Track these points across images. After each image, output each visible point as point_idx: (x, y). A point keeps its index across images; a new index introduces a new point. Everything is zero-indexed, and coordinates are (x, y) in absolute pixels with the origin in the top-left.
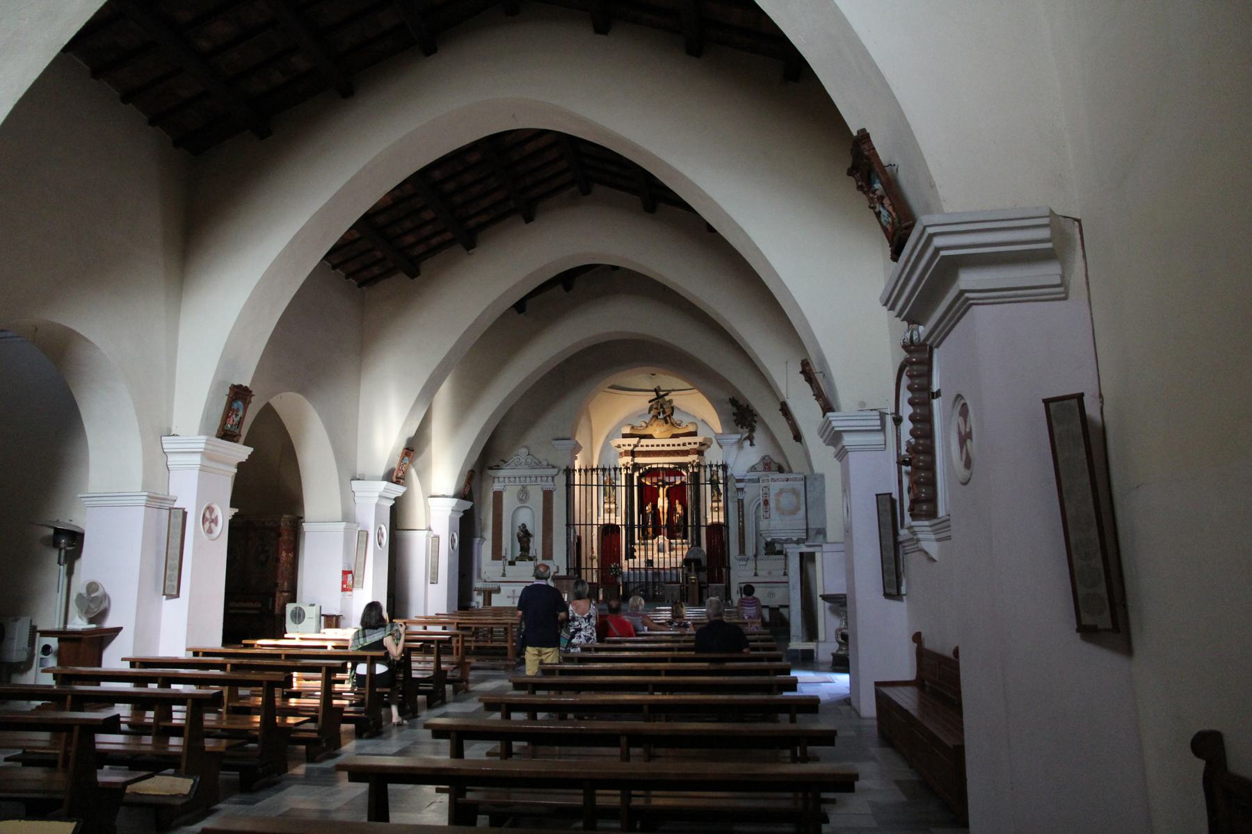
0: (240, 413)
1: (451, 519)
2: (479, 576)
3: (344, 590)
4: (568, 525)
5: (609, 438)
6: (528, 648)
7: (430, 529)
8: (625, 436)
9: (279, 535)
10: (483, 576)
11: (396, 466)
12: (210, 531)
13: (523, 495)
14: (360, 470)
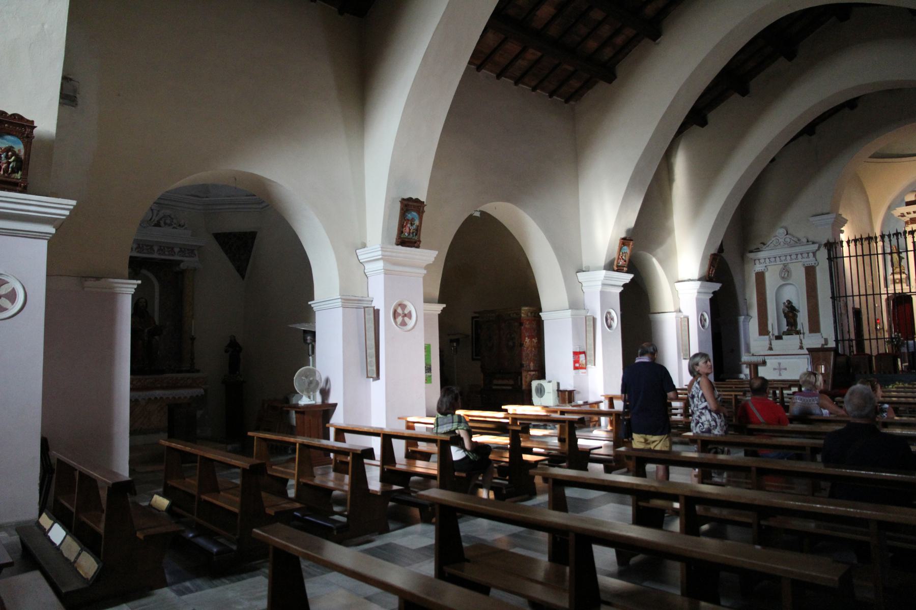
0: (417, 222)
1: (698, 300)
2: (748, 350)
3: (576, 368)
4: (833, 298)
5: (890, 208)
6: (635, 436)
7: (680, 311)
8: (908, 204)
9: (521, 324)
10: (753, 350)
11: (615, 255)
12: (404, 324)
13: (786, 273)
14: (585, 263)
